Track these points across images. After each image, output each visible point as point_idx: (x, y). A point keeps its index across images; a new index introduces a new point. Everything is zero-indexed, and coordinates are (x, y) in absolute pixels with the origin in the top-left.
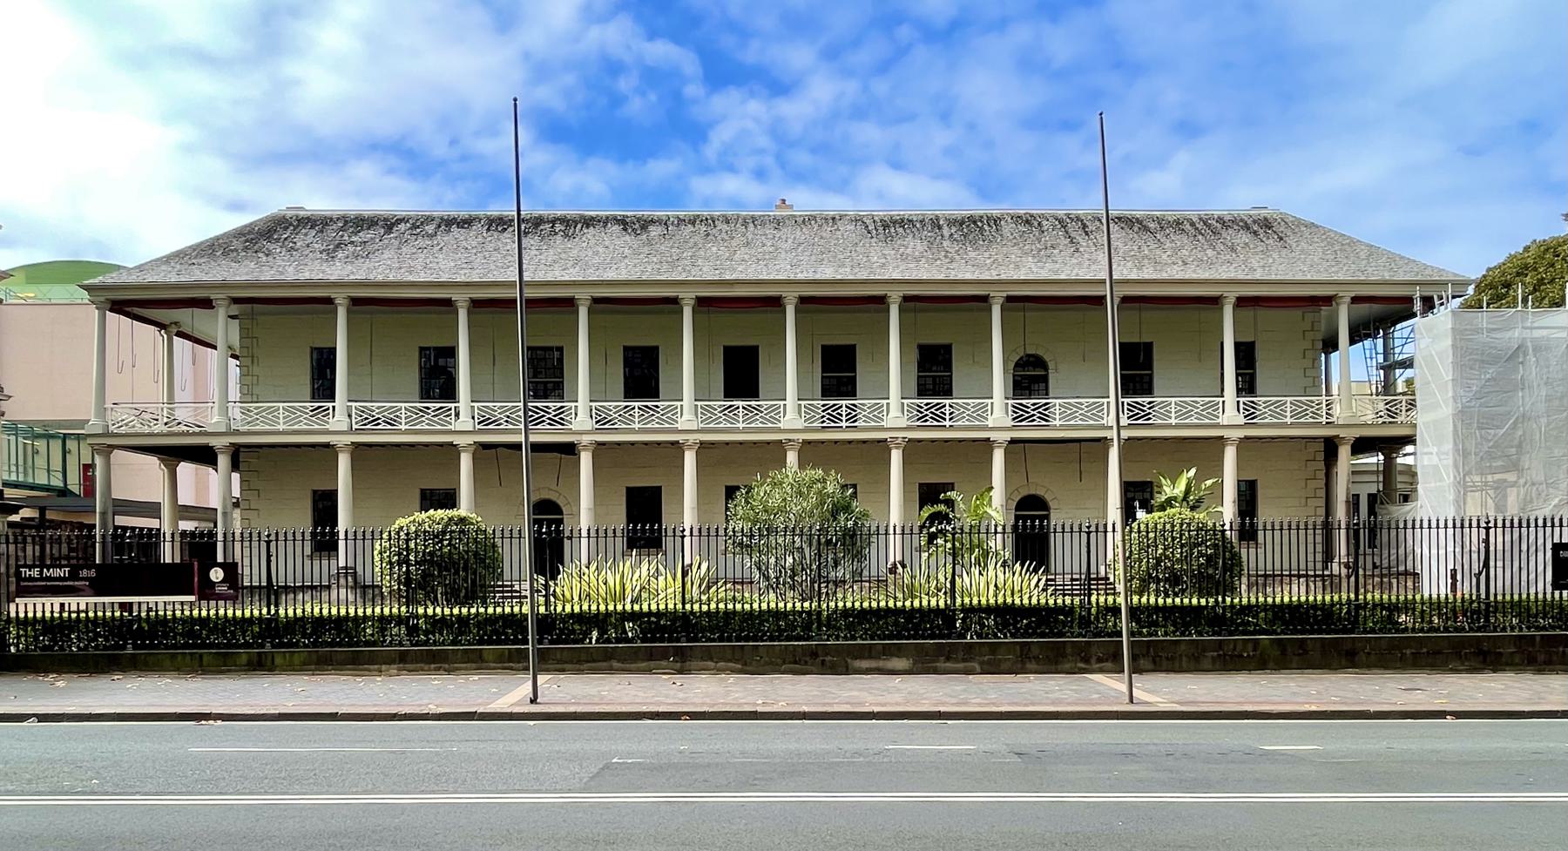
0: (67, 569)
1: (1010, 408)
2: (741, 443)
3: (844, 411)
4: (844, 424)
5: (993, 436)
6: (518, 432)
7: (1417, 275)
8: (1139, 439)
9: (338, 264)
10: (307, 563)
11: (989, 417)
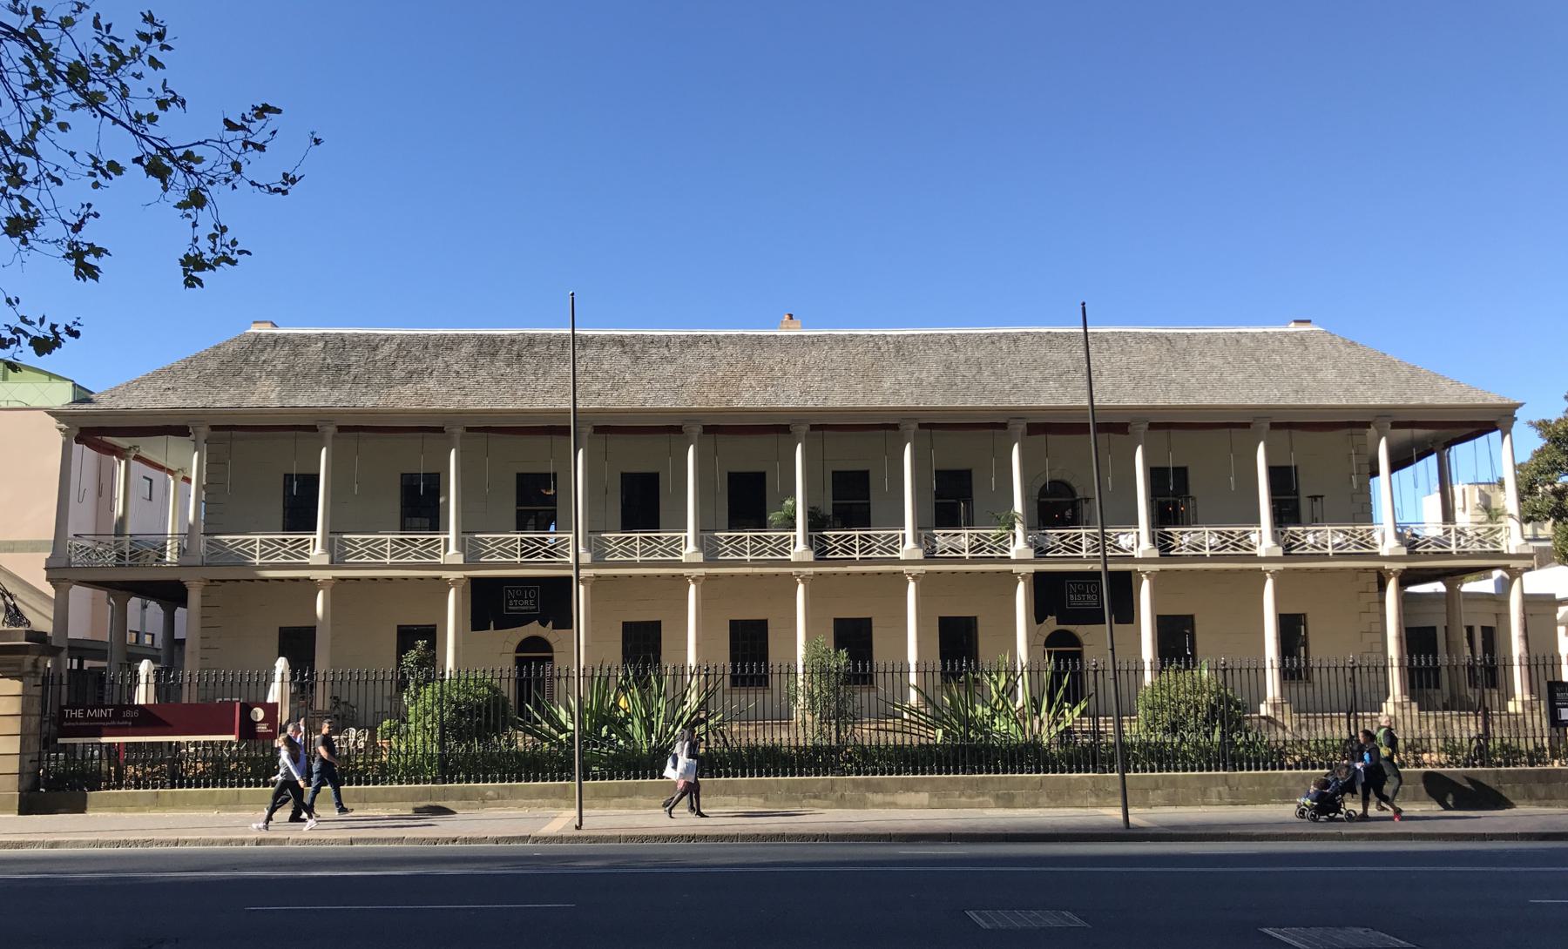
0: (110, 710)
1: (1157, 537)
2: (879, 574)
3: (857, 542)
4: (857, 556)
5: (1015, 568)
6: (570, 567)
7: (1119, 402)
8: (343, 579)
9: (323, 390)
10: (727, 697)
11: (1011, 548)
